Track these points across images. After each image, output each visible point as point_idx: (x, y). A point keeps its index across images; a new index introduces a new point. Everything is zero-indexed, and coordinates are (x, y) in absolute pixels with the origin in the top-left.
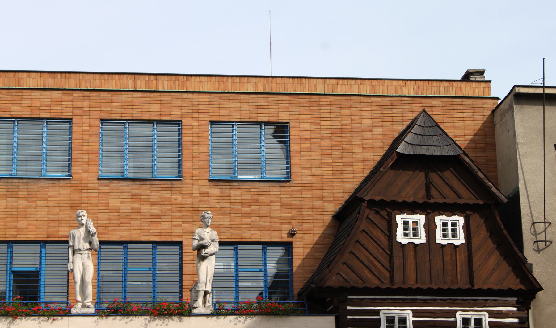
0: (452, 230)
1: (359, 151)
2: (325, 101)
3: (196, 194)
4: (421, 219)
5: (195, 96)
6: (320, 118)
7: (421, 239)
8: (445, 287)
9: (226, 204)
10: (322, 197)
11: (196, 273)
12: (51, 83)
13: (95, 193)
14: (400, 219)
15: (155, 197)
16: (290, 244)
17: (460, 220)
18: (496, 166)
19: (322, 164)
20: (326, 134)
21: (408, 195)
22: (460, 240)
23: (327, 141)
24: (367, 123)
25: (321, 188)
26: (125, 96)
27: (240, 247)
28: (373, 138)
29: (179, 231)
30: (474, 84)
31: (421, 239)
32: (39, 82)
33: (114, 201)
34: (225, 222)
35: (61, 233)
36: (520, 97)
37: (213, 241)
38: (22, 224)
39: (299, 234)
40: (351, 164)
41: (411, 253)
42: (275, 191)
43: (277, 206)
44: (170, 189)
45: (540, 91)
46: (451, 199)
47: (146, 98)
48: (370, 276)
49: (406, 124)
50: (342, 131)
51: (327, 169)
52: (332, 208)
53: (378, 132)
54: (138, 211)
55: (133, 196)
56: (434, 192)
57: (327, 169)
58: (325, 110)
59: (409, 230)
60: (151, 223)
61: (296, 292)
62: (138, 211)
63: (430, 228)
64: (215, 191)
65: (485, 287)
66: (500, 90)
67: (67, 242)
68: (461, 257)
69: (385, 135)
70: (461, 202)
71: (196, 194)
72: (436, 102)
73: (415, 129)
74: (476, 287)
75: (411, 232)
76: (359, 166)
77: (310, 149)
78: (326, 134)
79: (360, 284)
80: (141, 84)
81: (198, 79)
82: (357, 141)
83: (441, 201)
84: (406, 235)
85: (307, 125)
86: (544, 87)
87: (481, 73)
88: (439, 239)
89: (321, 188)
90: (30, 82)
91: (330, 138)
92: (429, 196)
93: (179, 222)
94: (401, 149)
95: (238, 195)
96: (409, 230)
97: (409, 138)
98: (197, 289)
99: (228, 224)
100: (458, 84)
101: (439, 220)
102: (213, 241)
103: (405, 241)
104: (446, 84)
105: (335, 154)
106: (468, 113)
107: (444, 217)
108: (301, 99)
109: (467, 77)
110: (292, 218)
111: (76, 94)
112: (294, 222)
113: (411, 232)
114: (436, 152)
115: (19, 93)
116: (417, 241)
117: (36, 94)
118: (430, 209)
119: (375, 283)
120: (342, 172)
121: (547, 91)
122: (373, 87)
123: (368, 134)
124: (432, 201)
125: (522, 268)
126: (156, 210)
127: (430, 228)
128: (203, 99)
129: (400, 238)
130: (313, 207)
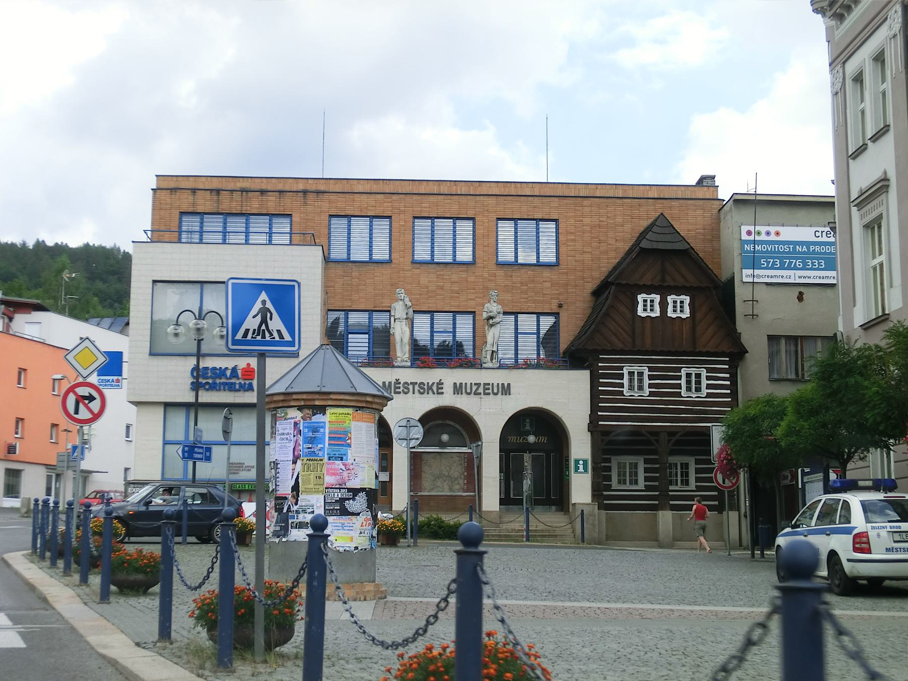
0: (680, 307)
1: (612, 242)
2: (586, 202)
3: (486, 275)
4: (657, 298)
5: (486, 198)
6: (583, 216)
7: (657, 313)
8: (674, 350)
9: (510, 283)
10: (583, 278)
11: (485, 336)
12: (375, 188)
13: (409, 274)
14: (640, 298)
15: (455, 277)
16: (558, 314)
17: (687, 299)
18: (720, 254)
19: (584, 252)
20: (587, 228)
21: (647, 281)
22: (686, 314)
23: (588, 234)
24: (619, 220)
25: (583, 271)
26: (432, 198)
27: (205, 286)
28: (623, 232)
29: (472, 303)
30: (706, 189)
31: (657, 313)
32: (367, 188)
33: (424, 280)
34: (508, 297)
35: (385, 305)
36: (740, 201)
37: (499, 313)
38: (355, 297)
39: (565, 307)
40: (606, 252)
41: (648, 325)
42: (546, 273)
43: (548, 285)
44: (467, 271)
45: (753, 198)
46: (681, 282)
47: (448, 200)
48: (616, 341)
49: (650, 221)
50: (599, 226)
51: (587, 257)
52: (590, 287)
53: (628, 227)
54: (442, 288)
55: (438, 276)
56: (668, 278)
57: (587, 257)
58: (587, 209)
59: (647, 305)
60: (452, 297)
61: (561, 351)
62: (442, 288)
63: (664, 305)
64: (500, 273)
65: (704, 350)
66: (724, 194)
67: (389, 311)
68: (686, 328)
69: (633, 230)
70: (688, 285)
71: (486, 275)
72: (674, 203)
73: (655, 229)
74: (698, 350)
75: (649, 308)
76: (612, 254)
77: (574, 240)
78: (587, 228)
79: (609, 347)
80: (444, 189)
81: (488, 184)
82: (611, 234)
83: (673, 284)
84: (645, 310)
85: (572, 221)
86: (756, 195)
87: (713, 177)
88: (670, 314)
89: (583, 271)
90: (359, 188)
91: (590, 232)
92: (663, 279)
93: (473, 296)
94: (644, 244)
95: (519, 276)
96: (647, 305)
97: (650, 236)
98: (85, 465)
99: (510, 298)
100: (692, 188)
101: (670, 299)
102: (499, 313)
103: (644, 315)
104: (683, 188)
105: (594, 244)
106: (699, 212)
107: (673, 296)
108: (568, 201)
109: (701, 181)
110: (559, 294)
111: (395, 197)
112: (561, 297)
113: (649, 308)
114: (669, 247)
115: (351, 196)
116: (653, 315)
117: (365, 196)
118: (664, 290)
119: (620, 346)
120: (599, 259)
121: (758, 198)
122: (625, 191)
123: (620, 229)
124: (665, 284)
125: (734, 337)
126: (456, 288)
127: (664, 305)
128: (492, 201)
129: (640, 312)
130: (576, 286)
